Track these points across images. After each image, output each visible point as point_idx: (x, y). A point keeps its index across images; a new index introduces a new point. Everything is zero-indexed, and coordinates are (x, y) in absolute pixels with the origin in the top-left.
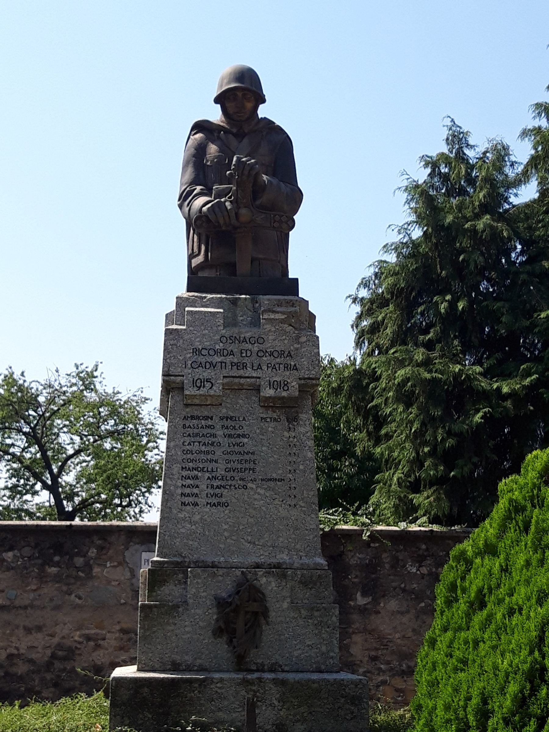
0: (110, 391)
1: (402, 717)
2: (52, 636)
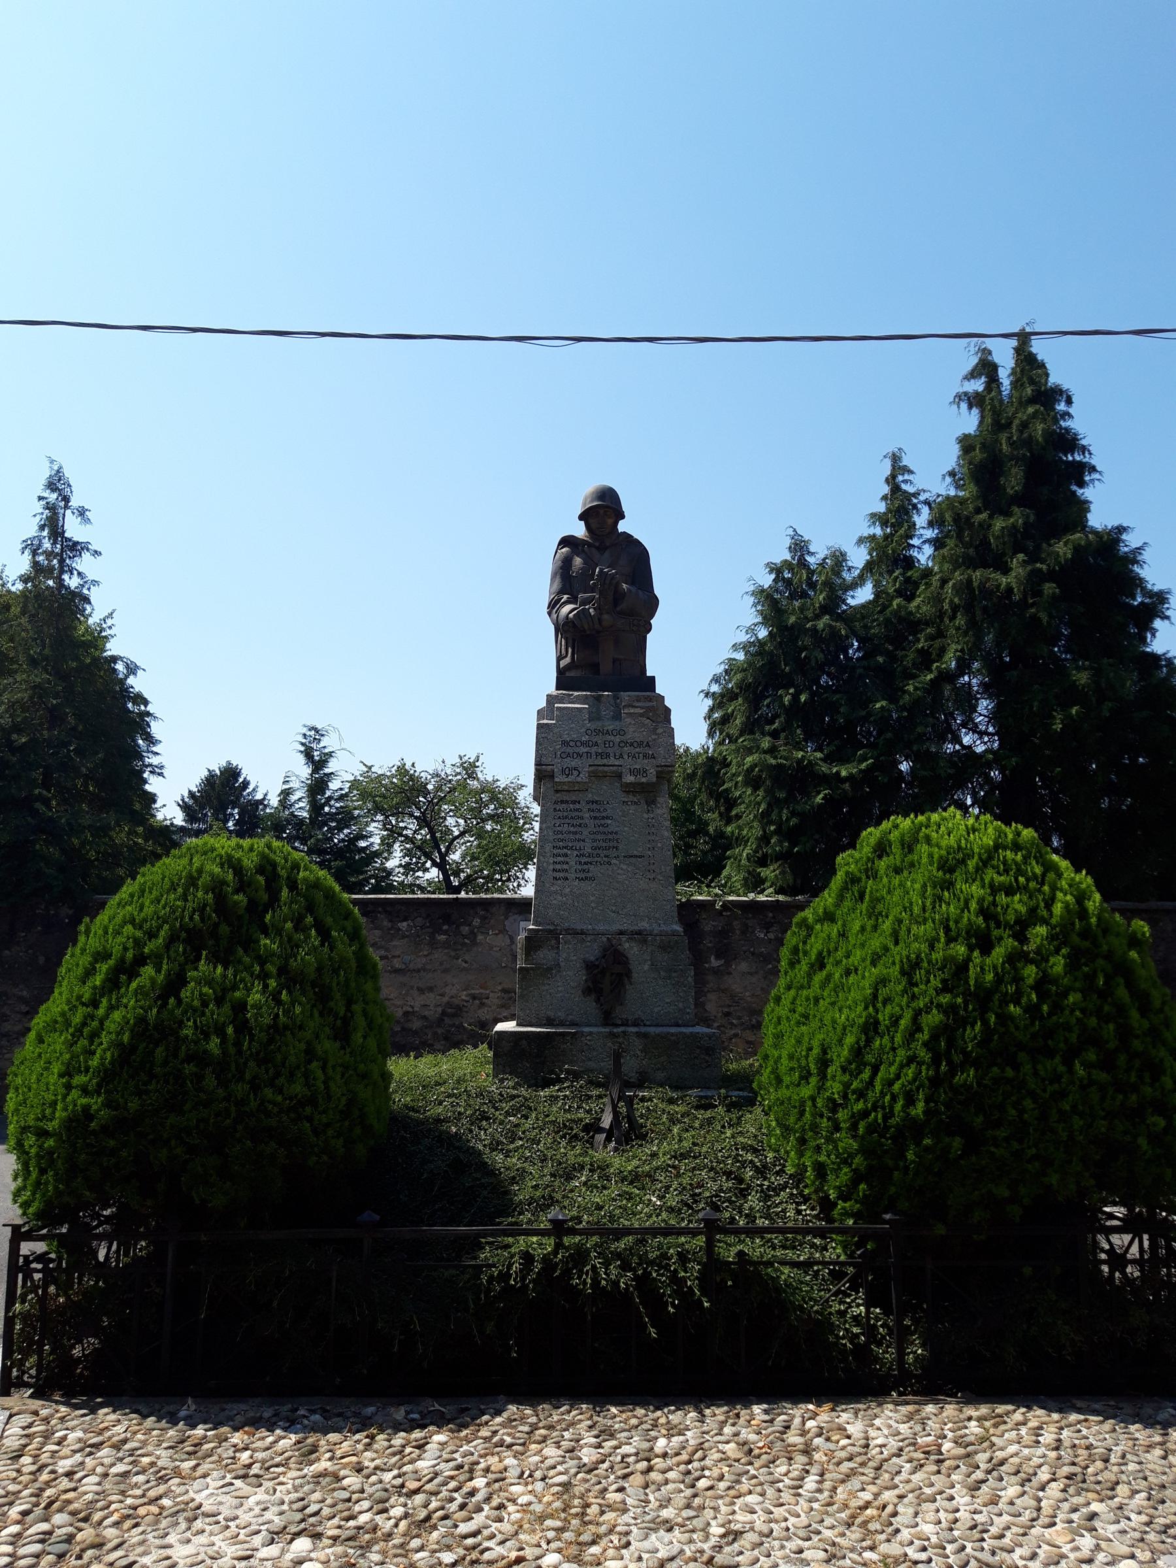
0: (490, 779)
1: (751, 1065)
2: (442, 995)
